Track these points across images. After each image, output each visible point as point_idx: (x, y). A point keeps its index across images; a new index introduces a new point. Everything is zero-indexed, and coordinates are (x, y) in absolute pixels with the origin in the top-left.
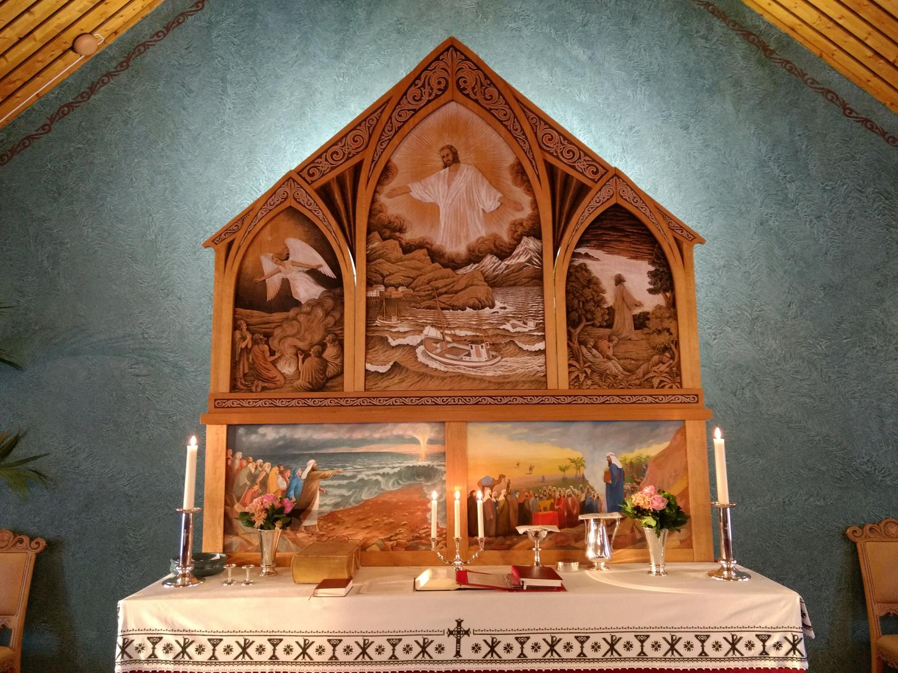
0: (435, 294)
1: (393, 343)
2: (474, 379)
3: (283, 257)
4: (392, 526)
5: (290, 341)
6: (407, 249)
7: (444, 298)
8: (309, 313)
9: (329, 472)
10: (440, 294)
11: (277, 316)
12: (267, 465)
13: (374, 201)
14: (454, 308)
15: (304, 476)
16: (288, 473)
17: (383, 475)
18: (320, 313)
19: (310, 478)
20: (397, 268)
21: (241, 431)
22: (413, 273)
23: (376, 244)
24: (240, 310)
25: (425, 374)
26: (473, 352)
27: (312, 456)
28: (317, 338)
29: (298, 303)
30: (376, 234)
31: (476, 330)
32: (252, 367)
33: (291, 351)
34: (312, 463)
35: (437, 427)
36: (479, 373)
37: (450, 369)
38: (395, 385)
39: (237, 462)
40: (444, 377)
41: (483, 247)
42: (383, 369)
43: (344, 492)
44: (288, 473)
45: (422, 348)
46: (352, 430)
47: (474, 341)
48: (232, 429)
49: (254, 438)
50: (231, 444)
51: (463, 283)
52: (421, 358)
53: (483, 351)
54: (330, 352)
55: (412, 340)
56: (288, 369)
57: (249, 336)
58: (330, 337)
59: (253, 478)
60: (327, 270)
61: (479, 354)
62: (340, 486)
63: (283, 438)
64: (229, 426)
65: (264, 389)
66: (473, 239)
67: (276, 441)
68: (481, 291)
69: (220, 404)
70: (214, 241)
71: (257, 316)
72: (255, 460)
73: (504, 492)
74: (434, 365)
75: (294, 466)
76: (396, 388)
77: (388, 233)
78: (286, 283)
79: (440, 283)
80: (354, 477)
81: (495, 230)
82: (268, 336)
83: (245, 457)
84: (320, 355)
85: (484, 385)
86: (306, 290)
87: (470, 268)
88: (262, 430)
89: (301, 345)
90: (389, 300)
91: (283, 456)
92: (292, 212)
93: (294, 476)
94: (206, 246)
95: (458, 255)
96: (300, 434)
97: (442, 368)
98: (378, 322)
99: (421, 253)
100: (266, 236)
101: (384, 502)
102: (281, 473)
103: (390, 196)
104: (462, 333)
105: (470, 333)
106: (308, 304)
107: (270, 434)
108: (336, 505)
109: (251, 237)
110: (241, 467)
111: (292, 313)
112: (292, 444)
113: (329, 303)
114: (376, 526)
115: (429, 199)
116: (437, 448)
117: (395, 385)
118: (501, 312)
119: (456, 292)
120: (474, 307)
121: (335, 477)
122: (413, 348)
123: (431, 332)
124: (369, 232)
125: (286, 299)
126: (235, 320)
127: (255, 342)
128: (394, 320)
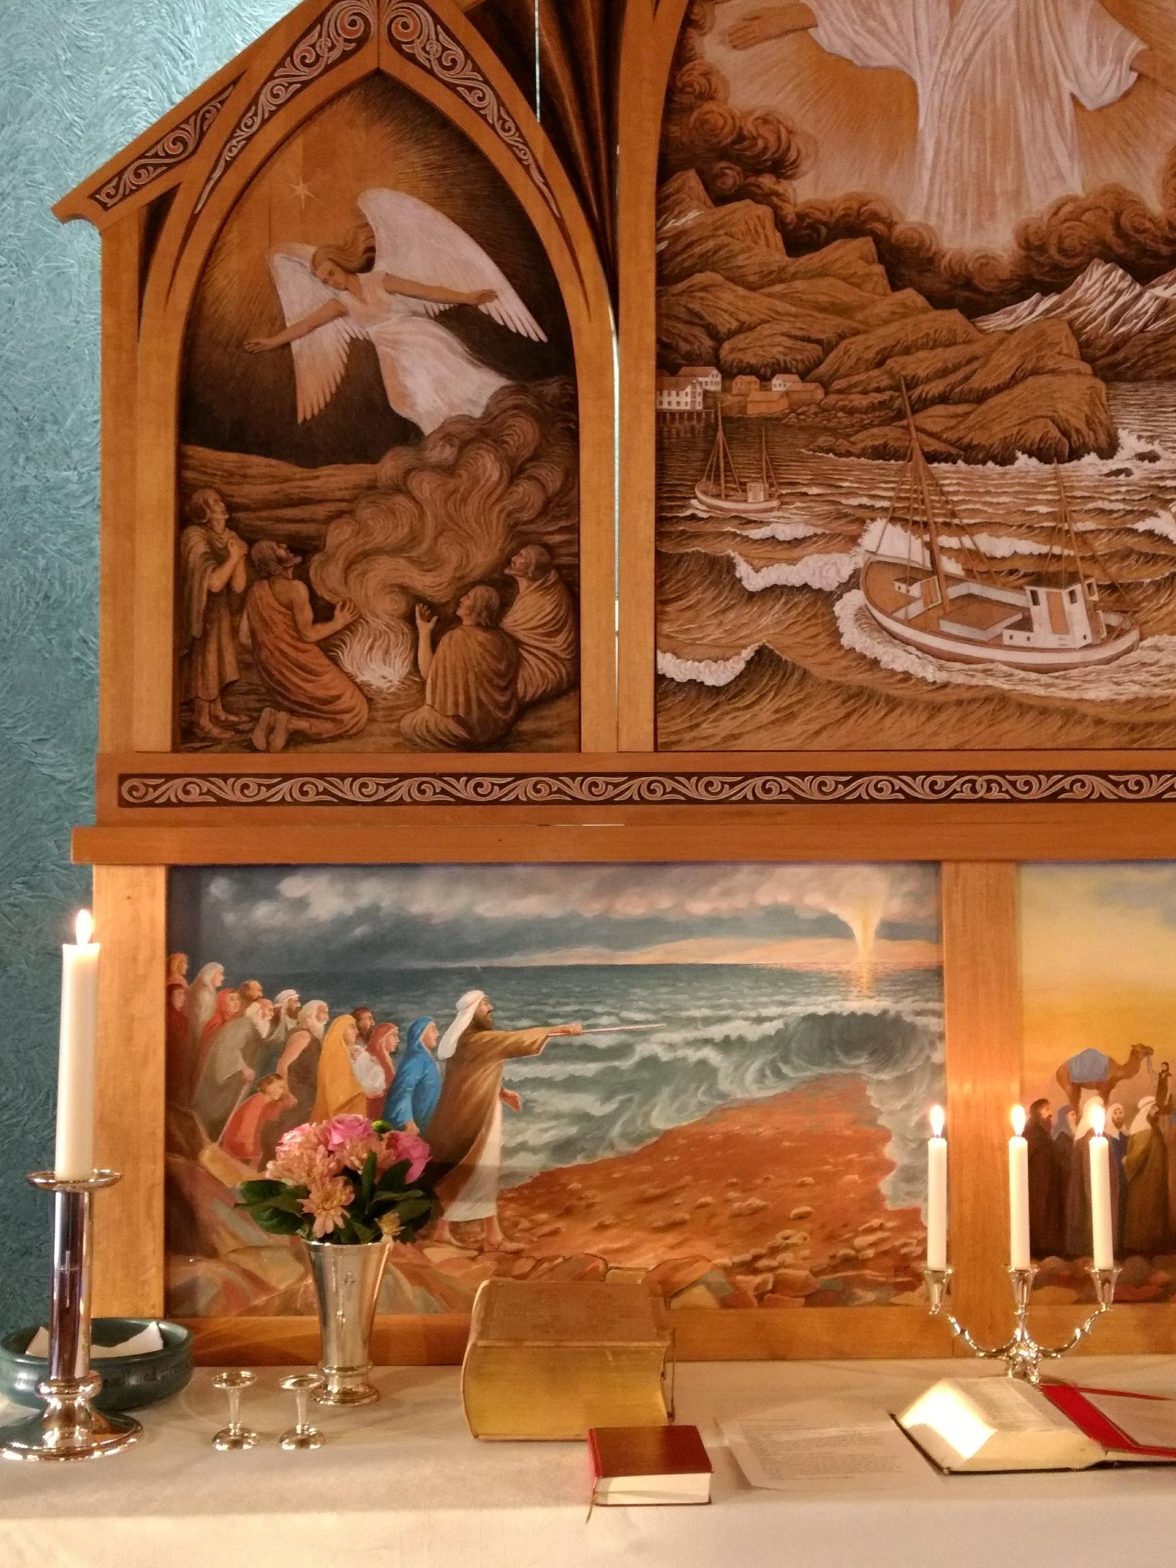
0: (903, 402)
1: (754, 581)
2: (1043, 710)
3: (355, 259)
4: (759, 1223)
5: (384, 569)
6: (803, 236)
7: (935, 418)
8: (448, 470)
9: (534, 1035)
10: (924, 404)
11: (335, 478)
12: (315, 1010)
13: (682, 56)
14: (971, 454)
15: (448, 1047)
16: (391, 1039)
17: (726, 1045)
18: (490, 467)
19: (469, 1052)
20: (764, 312)
21: (219, 888)
22: (826, 327)
23: (691, 217)
24: (200, 453)
25: (873, 691)
26: (1039, 613)
27: (474, 979)
28: (482, 559)
29: (407, 433)
30: (691, 180)
31: (1052, 534)
32: (252, 657)
33: (387, 607)
34: (472, 1001)
35: (913, 880)
36: (1059, 691)
37: (957, 675)
38: (762, 732)
39: (207, 1000)
40: (936, 702)
41: (1076, 235)
42: (718, 674)
43: (590, 1103)
44: (391, 1039)
45: (855, 599)
46: (611, 889)
47: (1044, 575)
48: (185, 882)
49: (263, 913)
50: (186, 935)
51: (1005, 363)
52: (853, 636)
53: (1077, 613)
54: (530, 610)
55: (822, 569)
56: (379, 667)
57: (237, 551)
58: (528, 556)
59: (265, 1054)
60: (512, 311)
61: (1060, 624)
62: (572, 1084)
63: (369, 914)
64: (173, 871)
65: (296, 739)
66: (1039, 203)
67: (343, 923)
68: (1071, 393)
69: (136, 793)
70: (96, 198)
71: (262, 475)
72: (270, 993)
73: (1147, 1104)
74: (897, 659)
75: (409, 1012)
76: (764, 740)
77: (731, 177)
78: (363, 354)
79: (921, 364)
80: (620, 1051)
81: (1116, 173)
82: (305, 549)
83: (234, 982)
84: (492, 619)
85: (1077, 734)
86: (438, 384)
87: (1027, 312)
88: (292, 886)
89: (425, 582)
90: (738, 426)
91: (368, 975)
92: (385, 94)
93: (409, 1049)
94: (67, 212)
95: (986, 261)
96: (431, 900)
97: (930, 672)
98: (700, 504)
99: (851, 253)
100: (289, 181)
101: (729, 1140)
102: (366, 1037)
103: (740, 39)
104: (1000, 546)
105: (1027, 546)
106: (446, 434)
107: (323, 900)
108: (562, 1148)
109: (233, 182)
110: (222, 1015)
111: (389, 467)
112: (402, 934)
113: (523, 433)
114: (703, 1223)
115: (882, 57)
116: (913, 954)
117: (762, 732)
118: (1141, 470)
119: (981, 397)
120: (1043, 454)
121: (554, 1052)
122: (826, 598)
123: (890, 541)
124: (664, 174)
125: (367, 418)
126: (184, 490)
127: (258, 570)
128: (756, 499)
